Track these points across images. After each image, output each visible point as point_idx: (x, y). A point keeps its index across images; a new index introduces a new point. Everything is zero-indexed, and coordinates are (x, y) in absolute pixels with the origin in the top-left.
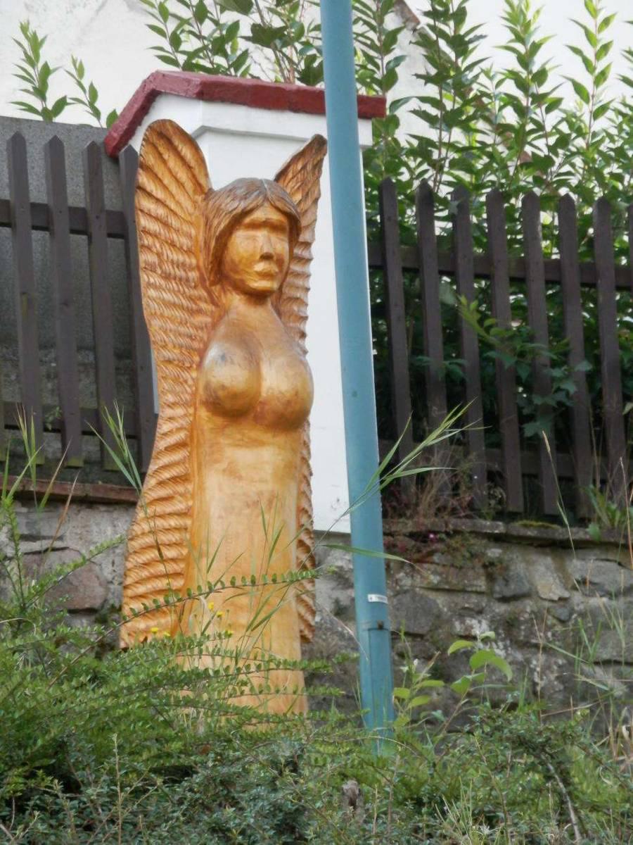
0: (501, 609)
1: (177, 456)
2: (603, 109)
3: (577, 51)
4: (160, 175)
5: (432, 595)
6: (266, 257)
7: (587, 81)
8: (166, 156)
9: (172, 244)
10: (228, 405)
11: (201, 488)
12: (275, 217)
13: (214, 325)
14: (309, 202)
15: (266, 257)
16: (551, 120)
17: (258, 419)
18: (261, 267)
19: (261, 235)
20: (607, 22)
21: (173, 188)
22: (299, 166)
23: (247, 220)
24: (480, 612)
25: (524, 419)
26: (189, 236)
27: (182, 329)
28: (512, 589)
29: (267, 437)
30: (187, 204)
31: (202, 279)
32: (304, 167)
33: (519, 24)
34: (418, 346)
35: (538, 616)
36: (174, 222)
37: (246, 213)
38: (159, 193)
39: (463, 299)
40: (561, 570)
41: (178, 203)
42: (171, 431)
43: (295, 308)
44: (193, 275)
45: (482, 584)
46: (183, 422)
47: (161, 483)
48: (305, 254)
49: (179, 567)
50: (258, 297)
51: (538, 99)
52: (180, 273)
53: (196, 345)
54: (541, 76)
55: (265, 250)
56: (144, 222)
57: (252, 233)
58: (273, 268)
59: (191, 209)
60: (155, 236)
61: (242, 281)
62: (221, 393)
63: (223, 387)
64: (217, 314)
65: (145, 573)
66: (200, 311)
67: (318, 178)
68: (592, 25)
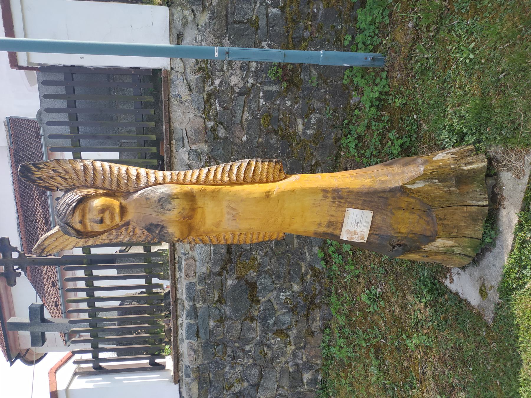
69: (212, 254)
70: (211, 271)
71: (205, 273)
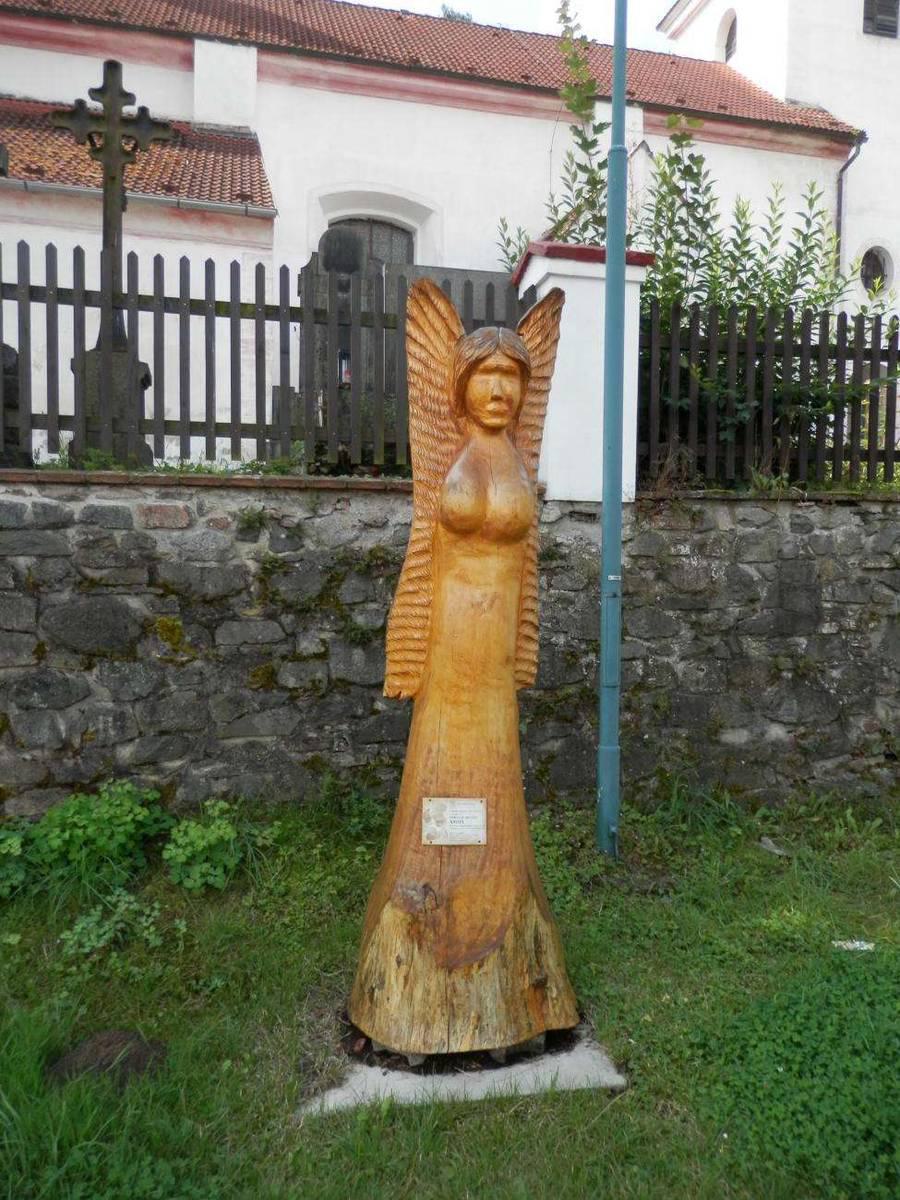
0: (697, 537)
1: (422, 560)
2: (775, 258)
3: (764, 229)
4: (421, 323)
5: (660, 533)
6: (496, 399)
7: (767, 245)
8: (425, 309)
9: (430, 382)
10: (458, 526)
11: (439, 588)
12: (506, 363)
13: (459, 451)
14: (549, 343)
15: (496, 399)
16: (749, 264)
17: (485, 535)
18: (492, 406)
19: (493, 379)
20: (781, 215)
21: (432, 336)
22: (539, 315)
23: (481, 366)
24: (686, 540)
25: (719, 430)
26: (443, 376)
27: (432, 455)
28: (705, 526)
29: (493, 548)
30: (442, 349)
31: (452, 412)
32: (543, 316)
33: (740, 214)
34: (666, 388)
35: (717, 541)
36: (433, 365)
37: (480, 360)
38: (422, 340)
39: (694, 366)
40: (732, 514)
41: (435, 348)
42: (418, 540)
43: (530, 434)
44: (445, 409)
45: (689, 524)
46: (427, 533)
47: (410, 580)
48: (544, 387)
49: (423, 645)
50: (494, 431)
51: (745, 253)
52: (435, 407)
53: (441, 469)
54: (747, 242)
55: (495, 393)
56: (411, 363)
57: (485, 377)
58: (504, 407)
59: (445, 354)
60: (419, 375)
61: (478, 418)
62: (451, 517)
63: (453, 513)
64: (461, 442)
65: (399, 646)
66: (447, 440)
67: (558, 323)
68: (773, 217)
69: (198, 565)
70: (158, 560)
71: (154, 547)
